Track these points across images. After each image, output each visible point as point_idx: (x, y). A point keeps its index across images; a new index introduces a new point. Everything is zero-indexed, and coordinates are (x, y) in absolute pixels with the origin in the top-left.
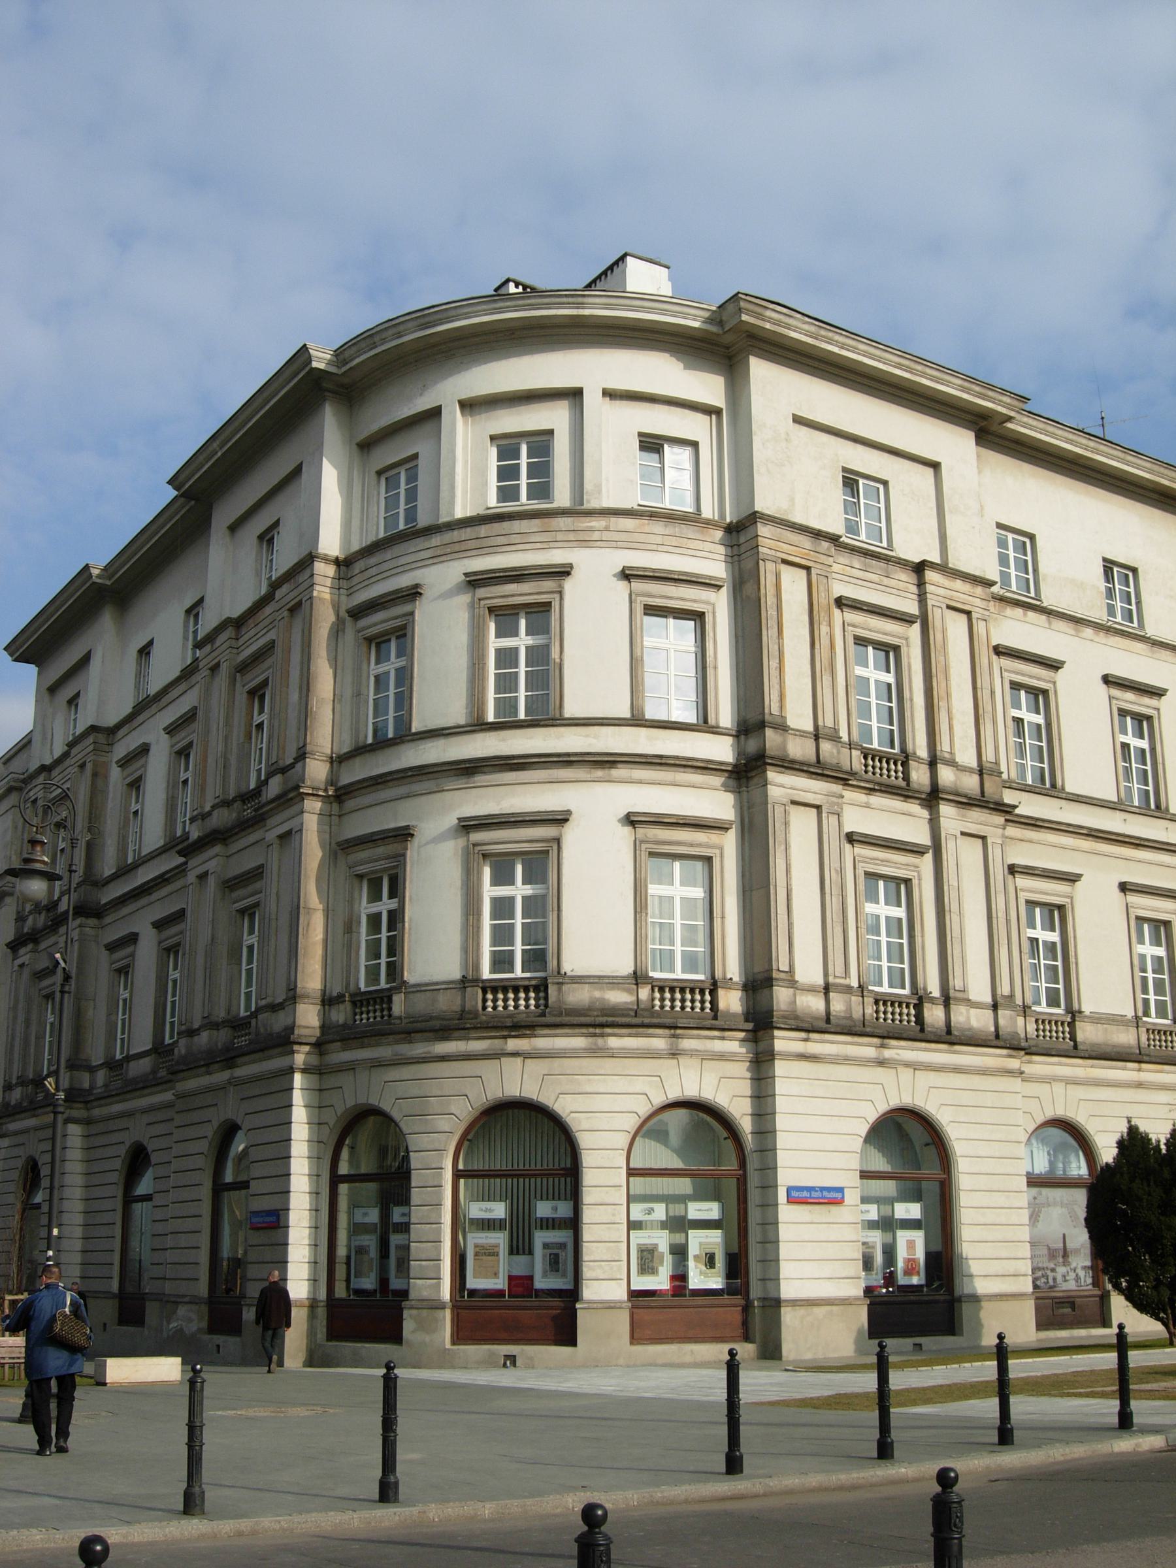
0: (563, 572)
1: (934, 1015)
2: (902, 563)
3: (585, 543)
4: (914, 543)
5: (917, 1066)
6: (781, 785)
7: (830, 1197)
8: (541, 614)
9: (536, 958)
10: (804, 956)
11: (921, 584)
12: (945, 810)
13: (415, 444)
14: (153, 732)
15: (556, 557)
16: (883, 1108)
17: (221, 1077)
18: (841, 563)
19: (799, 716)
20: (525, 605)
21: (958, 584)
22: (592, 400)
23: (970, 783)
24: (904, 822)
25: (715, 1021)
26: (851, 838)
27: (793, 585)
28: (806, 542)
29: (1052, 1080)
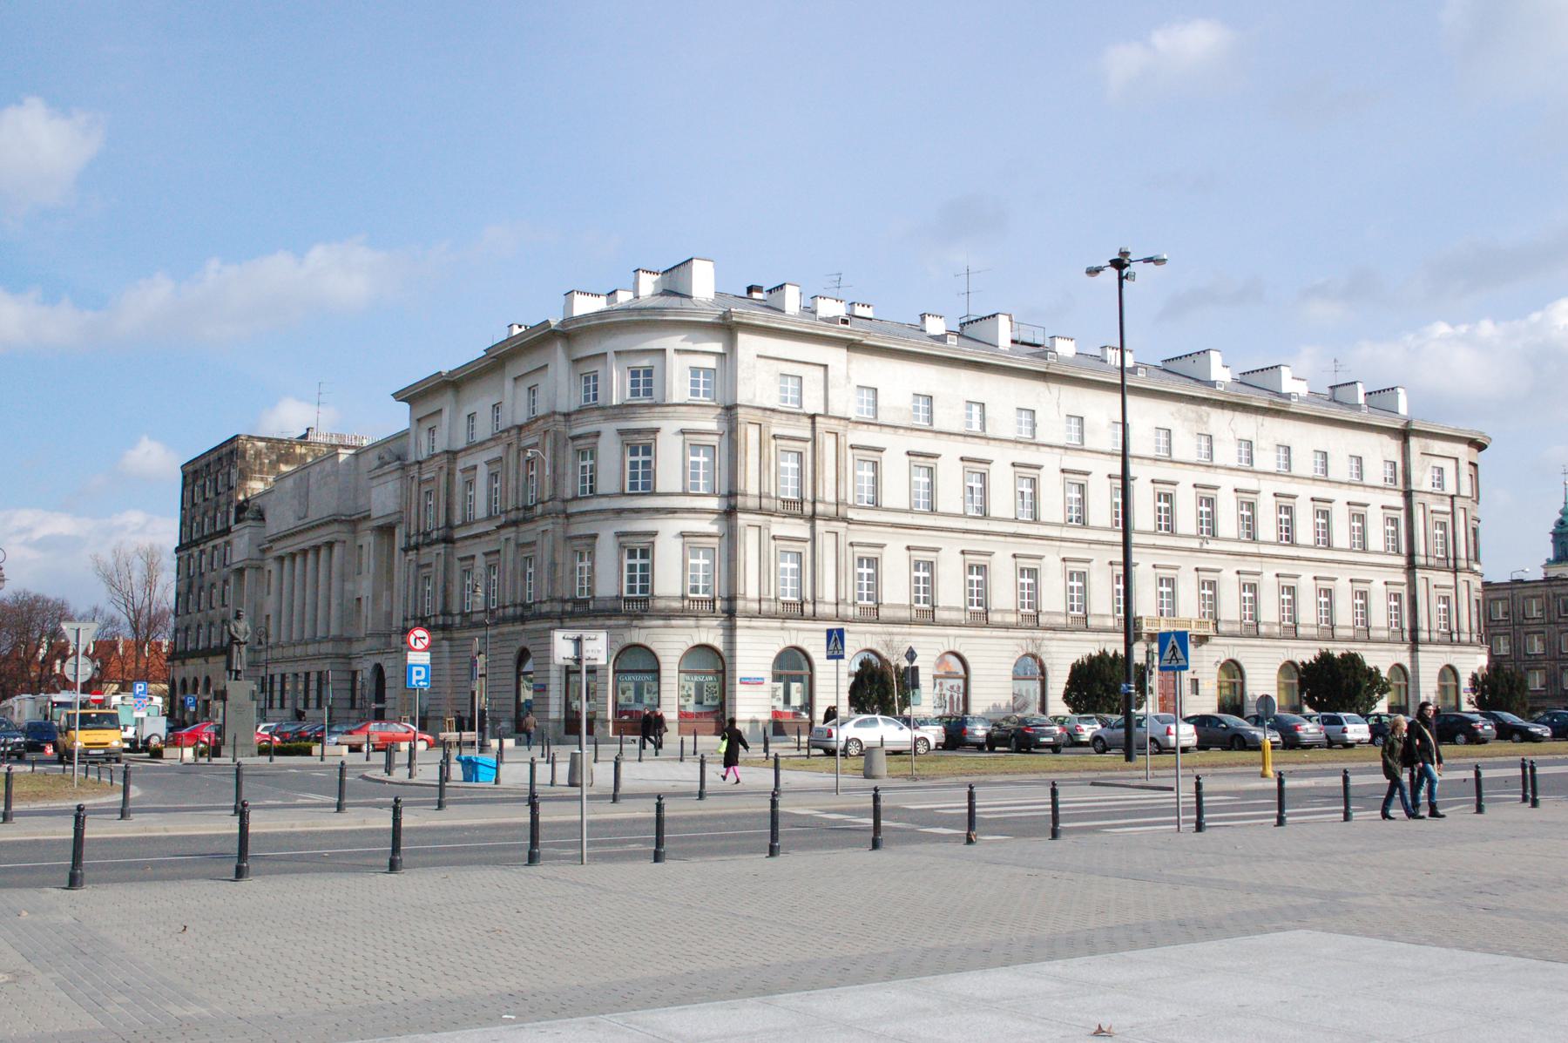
0: (657, 430)
1: (808, 608)
2: (805, 414)
3: (666, 418)
4: (813, 404)
5: (798, 630)
6: (742, 519)
7: (759, 682)
8: (647, 450)
9: (644, 589)
10: (750, 586)
11: (813, 423)
12: (818, 522)
13: (597, 367)
14: (480, 459)
15: (654, 424)
16: (783, 646)
17: (518, 627)
18: (776, 418)
19: (752, 488)
20: (641, 445)
21: (833, 421)
22: (670, 353)
23: (832, 509)
24: (800, 529)
25: (713, 613)
26: (774, 538)
27: (753, 432)
28: (759, 413)
29: (865, 633)
